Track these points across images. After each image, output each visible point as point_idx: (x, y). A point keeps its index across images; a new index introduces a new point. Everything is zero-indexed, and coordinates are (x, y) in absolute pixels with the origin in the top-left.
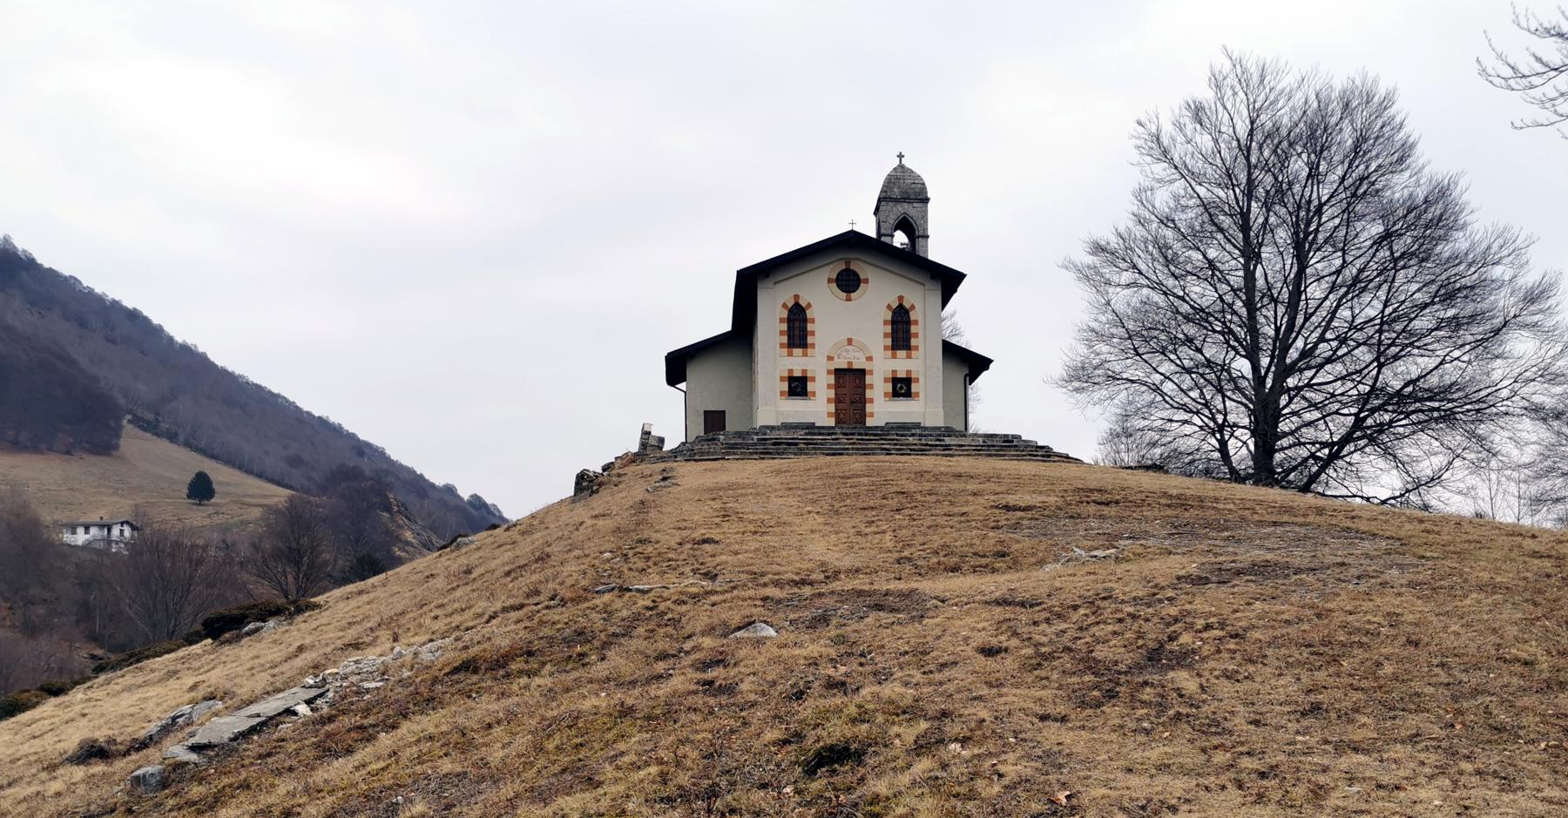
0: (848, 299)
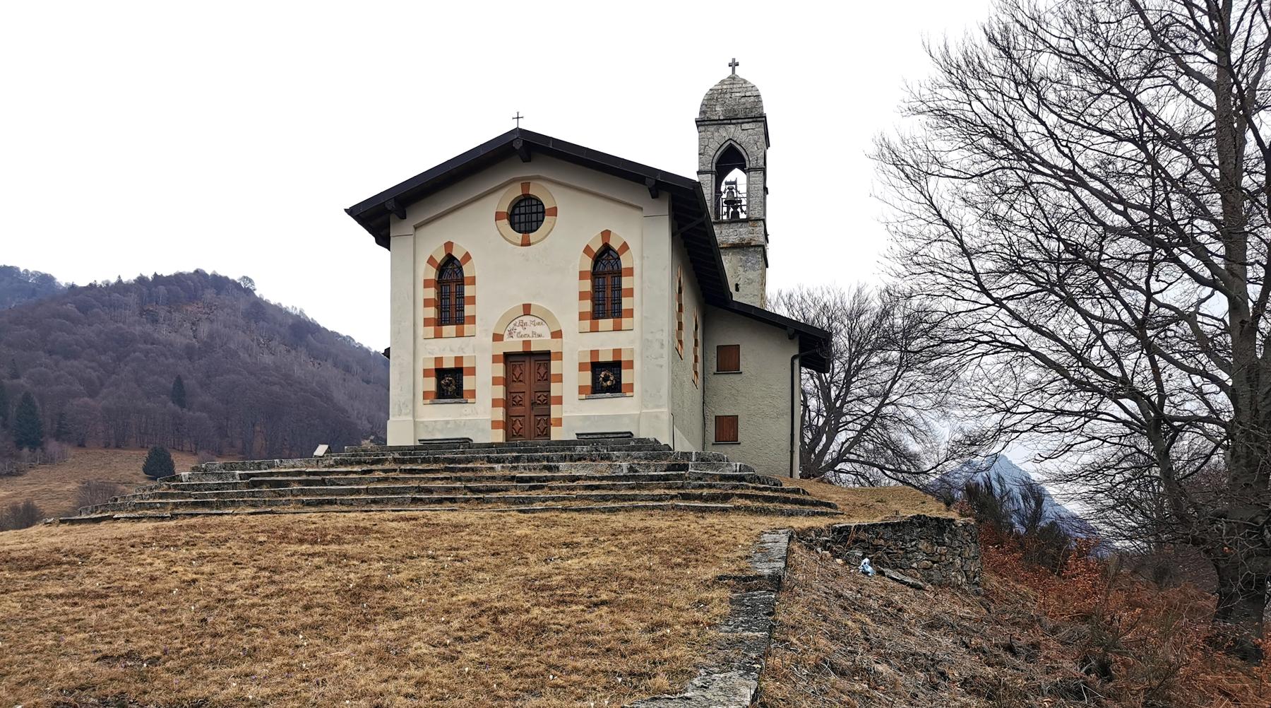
0: (526, 243)
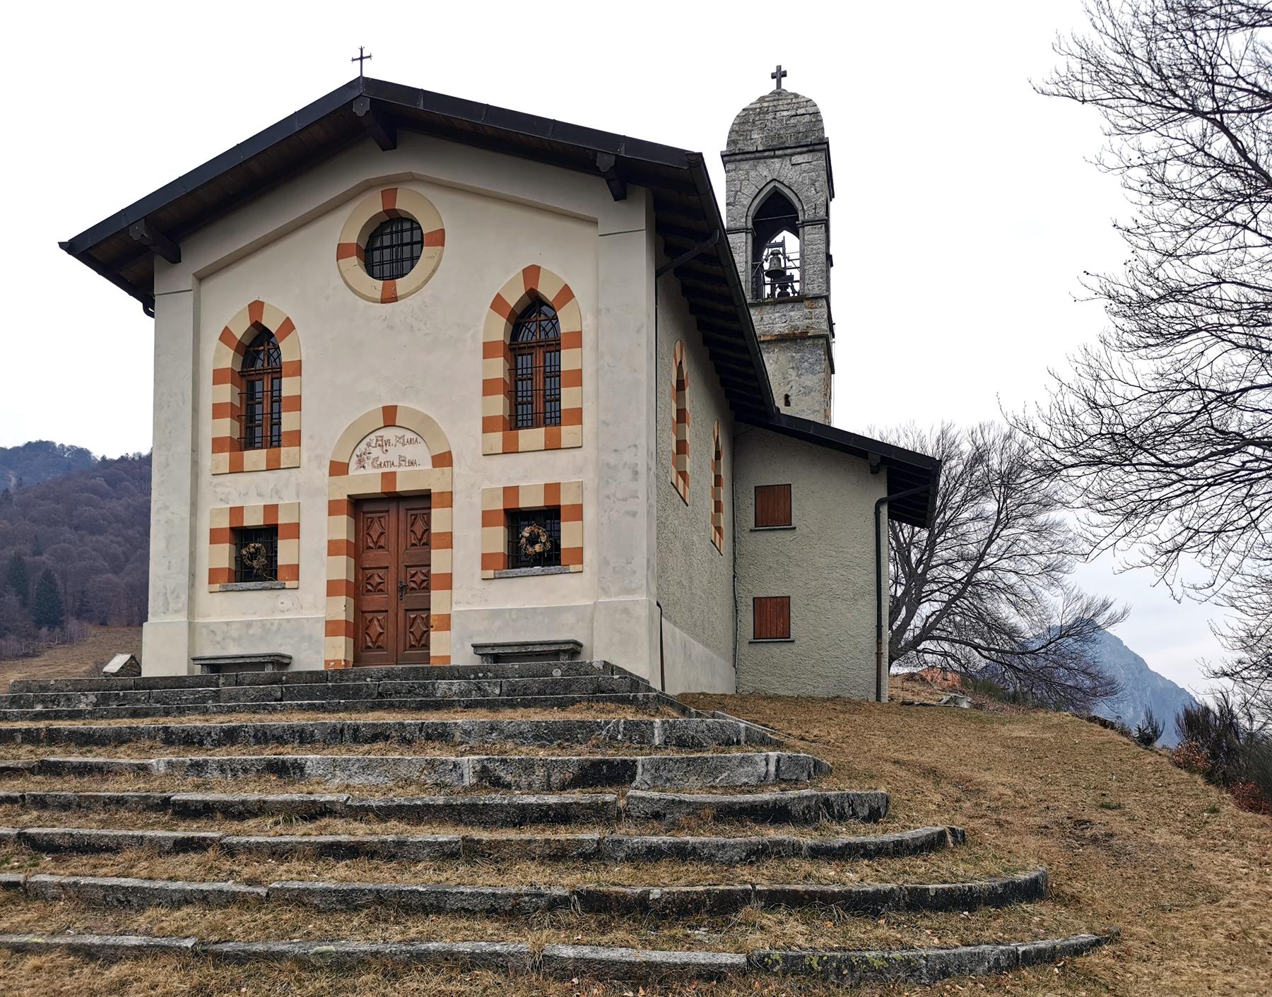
0: (390, 298)
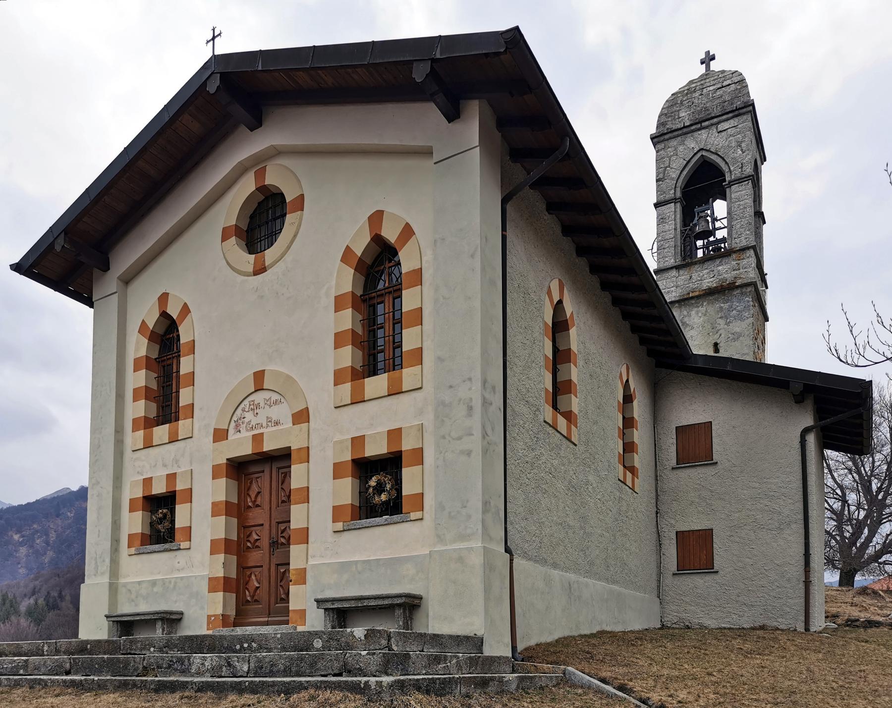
0: (260, 270)
